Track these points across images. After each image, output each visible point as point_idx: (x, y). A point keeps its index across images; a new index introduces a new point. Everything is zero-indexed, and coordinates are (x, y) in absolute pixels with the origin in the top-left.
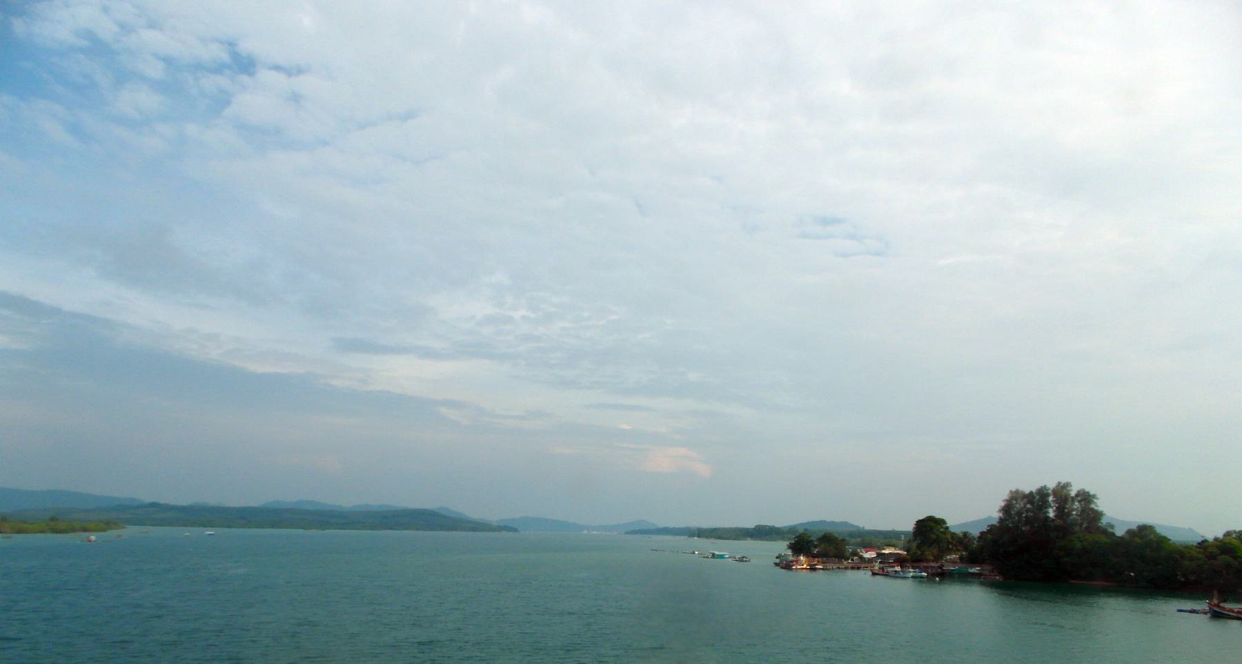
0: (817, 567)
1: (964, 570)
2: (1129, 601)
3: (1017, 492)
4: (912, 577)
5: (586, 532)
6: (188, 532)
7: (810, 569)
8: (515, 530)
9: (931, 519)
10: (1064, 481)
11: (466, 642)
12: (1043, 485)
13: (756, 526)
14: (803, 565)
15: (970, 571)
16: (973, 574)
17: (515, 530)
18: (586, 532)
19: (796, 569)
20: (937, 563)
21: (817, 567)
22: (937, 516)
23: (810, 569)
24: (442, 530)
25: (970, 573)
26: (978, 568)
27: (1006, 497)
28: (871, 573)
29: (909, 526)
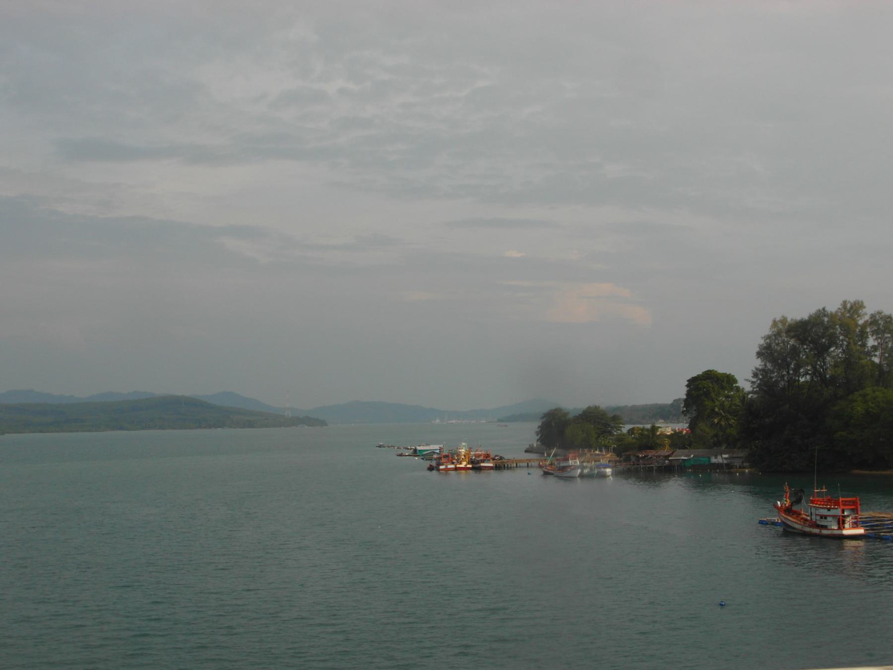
0: (482, 464)
1: (704, 460)
2: (630, 481)
3: (784, 321)
4: (582, 476)
5: (438, 421)
6: (888, 534)
7: (472, 469)
8: (323, 423)
9: (709, 376)
10: (852, 299)
11: (737, 656)
12: (821, 308)
13: (675, 401)
14: (461, 463)
15: (713, 460)
16: (718, 466)
17: (323, 423)
18: (438, 421)
19: (447, 470)
20: (666, 446)
21: (482, 464)
22: (721, 369)
23: (472, 469)
24: (200, 427)
25: (714, 464)
26: (726, 456)
27: (767, 331)
28: (540, 472)
29: (681, 393)
